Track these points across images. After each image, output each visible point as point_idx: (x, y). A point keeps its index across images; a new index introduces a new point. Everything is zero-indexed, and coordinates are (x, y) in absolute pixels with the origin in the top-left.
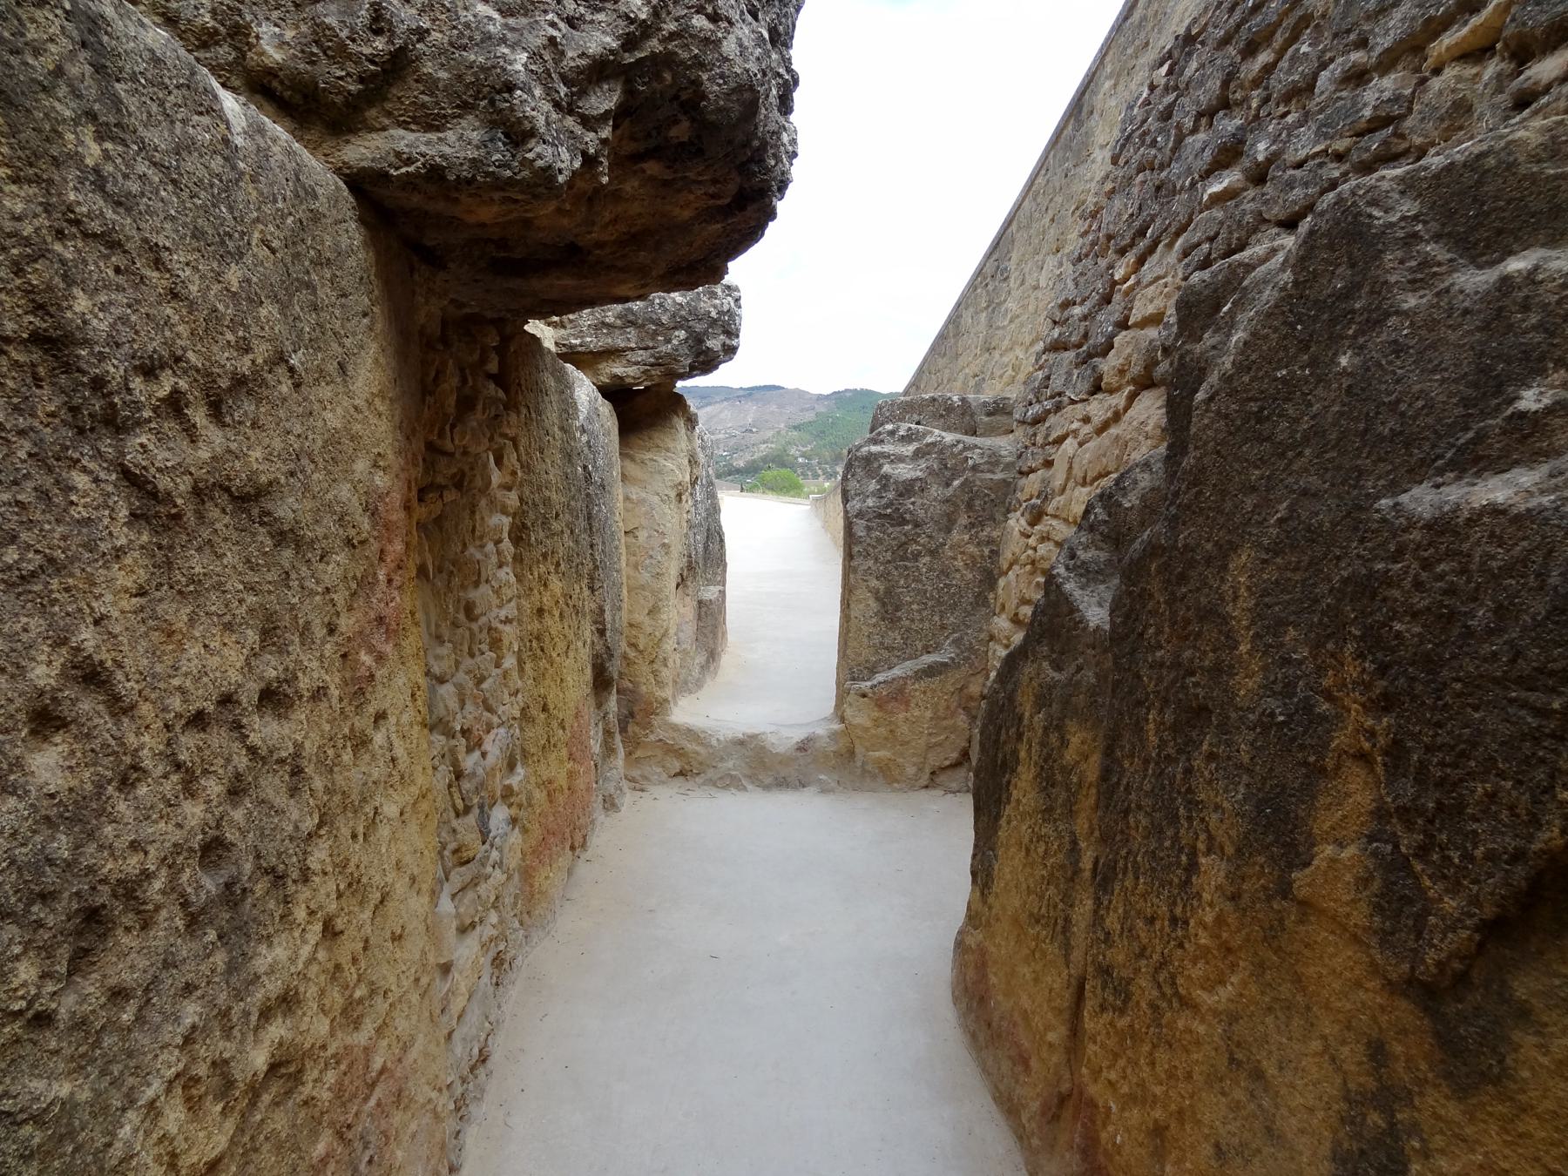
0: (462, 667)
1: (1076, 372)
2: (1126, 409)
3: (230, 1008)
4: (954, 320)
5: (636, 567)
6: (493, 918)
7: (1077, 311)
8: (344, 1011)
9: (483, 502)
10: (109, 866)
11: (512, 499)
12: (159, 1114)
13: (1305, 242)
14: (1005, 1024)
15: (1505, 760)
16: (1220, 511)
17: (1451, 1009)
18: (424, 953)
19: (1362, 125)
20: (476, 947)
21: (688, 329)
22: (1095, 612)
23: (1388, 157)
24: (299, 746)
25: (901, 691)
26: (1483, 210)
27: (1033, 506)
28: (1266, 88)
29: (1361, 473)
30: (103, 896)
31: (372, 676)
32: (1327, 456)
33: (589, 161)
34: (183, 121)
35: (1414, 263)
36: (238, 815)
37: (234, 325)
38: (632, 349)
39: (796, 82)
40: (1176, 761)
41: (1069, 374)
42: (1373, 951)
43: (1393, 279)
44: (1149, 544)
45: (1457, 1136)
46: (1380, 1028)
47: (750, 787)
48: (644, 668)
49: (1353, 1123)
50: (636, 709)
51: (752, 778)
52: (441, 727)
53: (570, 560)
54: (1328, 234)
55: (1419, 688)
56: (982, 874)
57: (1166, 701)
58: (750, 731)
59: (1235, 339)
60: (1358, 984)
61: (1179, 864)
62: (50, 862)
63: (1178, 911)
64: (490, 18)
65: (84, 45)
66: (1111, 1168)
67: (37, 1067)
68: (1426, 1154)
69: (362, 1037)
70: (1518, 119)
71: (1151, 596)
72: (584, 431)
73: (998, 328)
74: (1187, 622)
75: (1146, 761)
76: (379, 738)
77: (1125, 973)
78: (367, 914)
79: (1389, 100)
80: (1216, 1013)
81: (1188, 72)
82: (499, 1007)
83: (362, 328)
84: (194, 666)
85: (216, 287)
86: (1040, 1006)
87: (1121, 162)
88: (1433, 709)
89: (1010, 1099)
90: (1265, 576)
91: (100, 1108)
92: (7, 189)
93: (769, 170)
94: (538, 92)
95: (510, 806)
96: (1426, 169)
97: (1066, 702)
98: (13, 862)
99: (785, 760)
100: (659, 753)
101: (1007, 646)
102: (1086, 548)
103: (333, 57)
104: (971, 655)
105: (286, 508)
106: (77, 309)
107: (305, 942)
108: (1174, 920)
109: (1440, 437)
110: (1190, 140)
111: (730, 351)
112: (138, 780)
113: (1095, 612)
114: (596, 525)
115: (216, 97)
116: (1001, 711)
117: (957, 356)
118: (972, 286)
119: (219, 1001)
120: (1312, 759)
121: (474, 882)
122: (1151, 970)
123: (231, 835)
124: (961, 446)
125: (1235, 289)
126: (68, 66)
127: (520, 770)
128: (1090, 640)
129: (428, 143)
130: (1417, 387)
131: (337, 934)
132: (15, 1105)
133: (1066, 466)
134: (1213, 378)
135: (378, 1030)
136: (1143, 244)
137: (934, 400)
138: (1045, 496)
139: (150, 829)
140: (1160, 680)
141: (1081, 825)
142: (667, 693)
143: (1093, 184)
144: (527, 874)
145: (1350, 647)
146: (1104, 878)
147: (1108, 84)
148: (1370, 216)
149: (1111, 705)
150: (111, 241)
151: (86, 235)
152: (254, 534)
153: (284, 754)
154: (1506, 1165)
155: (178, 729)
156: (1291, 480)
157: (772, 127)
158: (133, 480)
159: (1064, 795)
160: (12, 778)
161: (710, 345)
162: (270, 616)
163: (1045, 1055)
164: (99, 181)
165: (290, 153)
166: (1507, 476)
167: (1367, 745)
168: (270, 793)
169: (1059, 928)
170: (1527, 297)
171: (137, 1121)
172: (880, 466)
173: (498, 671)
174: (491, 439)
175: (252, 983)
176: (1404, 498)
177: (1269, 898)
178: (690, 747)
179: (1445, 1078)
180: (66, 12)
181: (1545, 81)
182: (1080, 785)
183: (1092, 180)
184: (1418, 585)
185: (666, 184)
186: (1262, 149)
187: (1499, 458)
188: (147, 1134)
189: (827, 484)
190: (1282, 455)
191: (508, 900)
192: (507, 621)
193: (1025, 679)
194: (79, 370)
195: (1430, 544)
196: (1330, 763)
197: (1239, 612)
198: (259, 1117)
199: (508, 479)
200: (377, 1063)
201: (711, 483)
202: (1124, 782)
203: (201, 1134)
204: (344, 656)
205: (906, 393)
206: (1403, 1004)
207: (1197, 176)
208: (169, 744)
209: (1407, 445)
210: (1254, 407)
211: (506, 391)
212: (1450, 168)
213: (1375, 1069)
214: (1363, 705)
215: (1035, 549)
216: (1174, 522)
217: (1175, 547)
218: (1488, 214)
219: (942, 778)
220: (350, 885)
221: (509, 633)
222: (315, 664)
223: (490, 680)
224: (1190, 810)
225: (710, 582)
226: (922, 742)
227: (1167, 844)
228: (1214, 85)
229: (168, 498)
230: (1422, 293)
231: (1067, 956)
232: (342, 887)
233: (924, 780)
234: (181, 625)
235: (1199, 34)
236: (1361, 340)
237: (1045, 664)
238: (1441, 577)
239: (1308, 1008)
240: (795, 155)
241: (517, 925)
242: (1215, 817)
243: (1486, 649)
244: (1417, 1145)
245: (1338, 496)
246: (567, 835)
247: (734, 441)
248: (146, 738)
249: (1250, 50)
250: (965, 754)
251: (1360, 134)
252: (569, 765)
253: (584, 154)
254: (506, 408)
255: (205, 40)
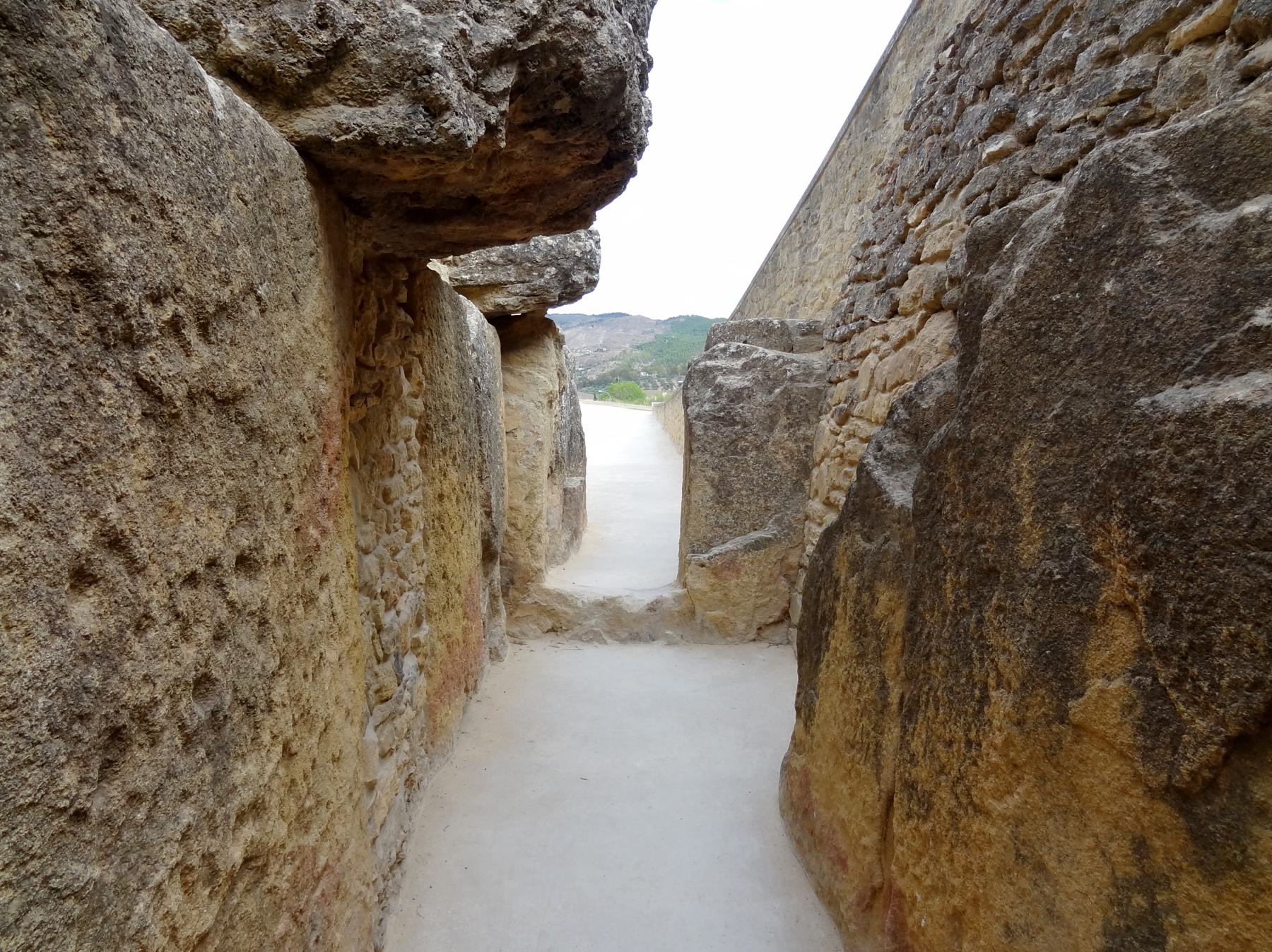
0: (381, 541)
1: (876, 300)
2: (919, 330)
3: (215, 812)
4: (773, 258)
5: (515, 461)
6: (406, 746)
7: (877, 249)
8: (298, 818)
9: (396, 408)
10: (128, 694)
11: (418, 405)
12: (164, 895)
13: (1075, 191)
14: (825, 831)
15: (1246, 607)
16: (1005, 409)
17: (1202, 810)
18: (356, 773)
19: (1115, 96)
20: (394, 771)
21: (558, 266)
22: (900, 492)
23: (1137, 123)
24: (265, 602)
25: (733, 561)
26: (1219, 165)
27: (841, 410)
28: (1034, 67)
29: (1123, 377)
30: (124, 718)
31: (318, 546)
32: (1095, 364)
33: (491, 129)
34: (181, 100)
35: (1165, 208)
36: (221, 656)
37: (219, 262)
38: (512, 283)
39: (651, 64)
40: (970, 613)
41: (870, 301)
42: (1136, 764)
43: (1148, 221)
44: (947, 442)
45: (1207, 913)
46: (1143, 827)
47: (609, 641)
48: (522, 544)
49: (1120, 904)
50: (516, 577)
51: (612, 633)
52: (366, 590)
53: (464, 455)
54: (1094, 184)
55: (1174, 550)
56: (805, 709)
57: (961, 565)
58: (609, 595)
59: (1016, 270)
60: (1124, 791)
61: (973, 696)
62: (86, 690)
63: (973, 735)
64: (413, 15)
65: (109, 40)
66: (916, 947)
67: (76, 853)
68: (1182, 928)
69: (311, 839)
70: (1245, 90)
71: (948, 479)
72: (474, 350)
73: (810, 264)
74: (979, 500)
75: (945, 614)
76: (323, 597)
77: (927, 787)
78: (314, 740)
79: (1137, 76)
80: (1004, 817)
81: (968, 54)
82: (410, 819)
83: (310, 265)
84: (189, 536)
85: (205, 232)
86: (856, 816)
87: (913, 127)
88: (1185, 567)
89: (830, 893)
90: (1044, 462)
91: (121, 889)
92: (54, 154)
93: (632, 136)
94: (451, 74)
95: (418, 655)
96: (1174, 132)
97: (875, 568)
98: (60, 689)
99: (638, 619)
100: (535, 614)
101: (820, 525)
102: (891, 442)
103: (287, 47)
104: (792, 532)
105: (256, 410)
106: (105, 249)
107: (269, 760)
108: (969, 743)
109: (1189, 348)
110: (970, 109)
111: (592, 284)
112: (148, 626)
113: (900, 492)
114: (484, 426)
115: (203, 80)
116: (820, 576)
117: (776, 287)
118: (788, 230)
119: (207, 806)
120: (1084, 609)
121: (392, 717)
122: (950, 784)
123: (216, 673)
124: (781, 361)
125: (1015, 230)
126: (97, 57)
127: (425, 626)
128: (896, 516)
129: (363, 116)
130: (1169, 308)
131: (292, 755)
132: (61, 883)
133: (869, 376)
134: (999, 302)
135: (323, 835)
136: (931, 195)
137: (758, 323)
138: (851, 401)
139: (157, 667)
140: (956, 547)
141: (889, 667)
142: (541, 564)
143: (889, 146)
144: (431, 711)
145: (1116, 519)
146: (909, 711)
147: (901, 64)
148: (1129, 170)
149: (915, 569)
150: (130, 197)
151: (112, 191)
152: (231, 431)
153: (254, 608)
154: (1248, 936)
155: (177, 586)
156: (1064, 383)
157: (635, 101)
158: (144, 386)
159: (874, 643)
160: (58, 622)
161: (575, 280)
162: (243, 497)
163: (860, 855)
164: (120, 148)
165: (256, 125)
166: (1245, 378)
167: (1130, 597)
168: (243, 639)
169: (871, 752)
170: (1260, 234)
171: (148, 900)
172: (715, 378)
173: (408, 545)
174: (402, 356)
175: (231, 792)
176: (1160, 397)
177: (1049, 724)
178: (560, 608)
179: (1197, 866)
180: (97, 14)
181: (1266, 60)
182: (888, 634)
183: (887, 142)
184: (1172, 467)
185: (549, 147)
186: (1031, 116)
187: (1238, 364)
188: (156, 910)
189: (664, 394)
190: (1057, 364)
191: (416, 733)
192: (415, 504)
193: (840, 549)
194: (106, 298)
195: (1182, 434)
196: (1099, 613)
197: (1022, 491)
198: (235, 901)
199: (416, 389)
200: (322, 861)
201: (573, 393)
202: (926, 631)
203: (194, 913)
204: (297, 530)
205: (733, 317)
206: (1162, 807)
207: (976, 139)
208: (171, 598)
209: (1162, 355)
210: (1033, 325)
211: (413, 317)
212: (1194, 131)
213: (1139, 860)
214: (1127, 565)
215: (843, 444)
216: (966, 420)
217: (967, 440)
218: (1226, 167)
219: (766, 633)
220: (302, 715)
221: (417, 514)
222: (277, 536)
223: (402, 552)
224: (982, 653)
225: (573, 474)
226: (750, 603)
227: (963, 680)
228: (990, 64)
229: (170, 401)
230: (1172, 231)
231: (878, 775)
232: (296, 717)
233: (752, 634)
234: (179, 502)
235: (977, 23)
236: (1122, 270)
237: (858, 537)
238: (1191, 460)
239: (1082, 812)
240: (650, 123)
241: (423, 753)
242: (1003, 658)
243: (1229, 517)
244: (1174, 921)
245: (1104, 397)
246: (462, 680)
247: (587, 359)
248: (154, 593)
249: (1020, 36)
250: (786, 614)
251: (1113, 104)
252: (464, 623)
253: (487, 123)
254: (413, 330)
255: (184, 34)
